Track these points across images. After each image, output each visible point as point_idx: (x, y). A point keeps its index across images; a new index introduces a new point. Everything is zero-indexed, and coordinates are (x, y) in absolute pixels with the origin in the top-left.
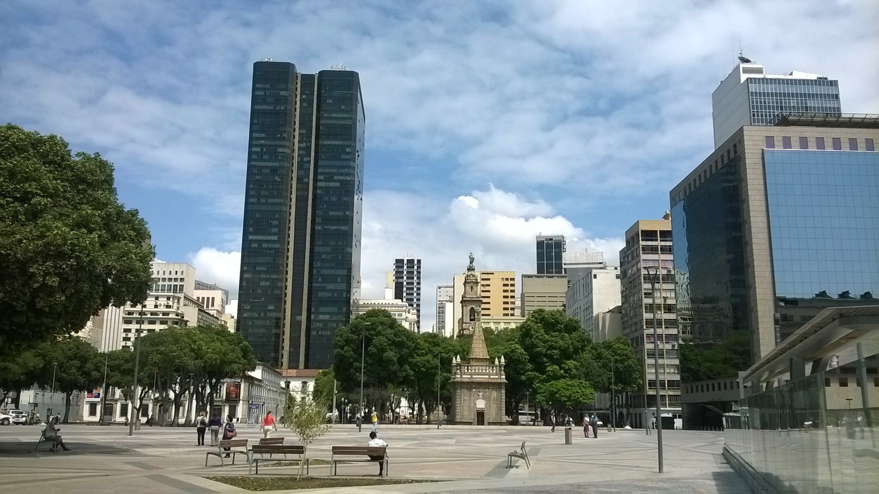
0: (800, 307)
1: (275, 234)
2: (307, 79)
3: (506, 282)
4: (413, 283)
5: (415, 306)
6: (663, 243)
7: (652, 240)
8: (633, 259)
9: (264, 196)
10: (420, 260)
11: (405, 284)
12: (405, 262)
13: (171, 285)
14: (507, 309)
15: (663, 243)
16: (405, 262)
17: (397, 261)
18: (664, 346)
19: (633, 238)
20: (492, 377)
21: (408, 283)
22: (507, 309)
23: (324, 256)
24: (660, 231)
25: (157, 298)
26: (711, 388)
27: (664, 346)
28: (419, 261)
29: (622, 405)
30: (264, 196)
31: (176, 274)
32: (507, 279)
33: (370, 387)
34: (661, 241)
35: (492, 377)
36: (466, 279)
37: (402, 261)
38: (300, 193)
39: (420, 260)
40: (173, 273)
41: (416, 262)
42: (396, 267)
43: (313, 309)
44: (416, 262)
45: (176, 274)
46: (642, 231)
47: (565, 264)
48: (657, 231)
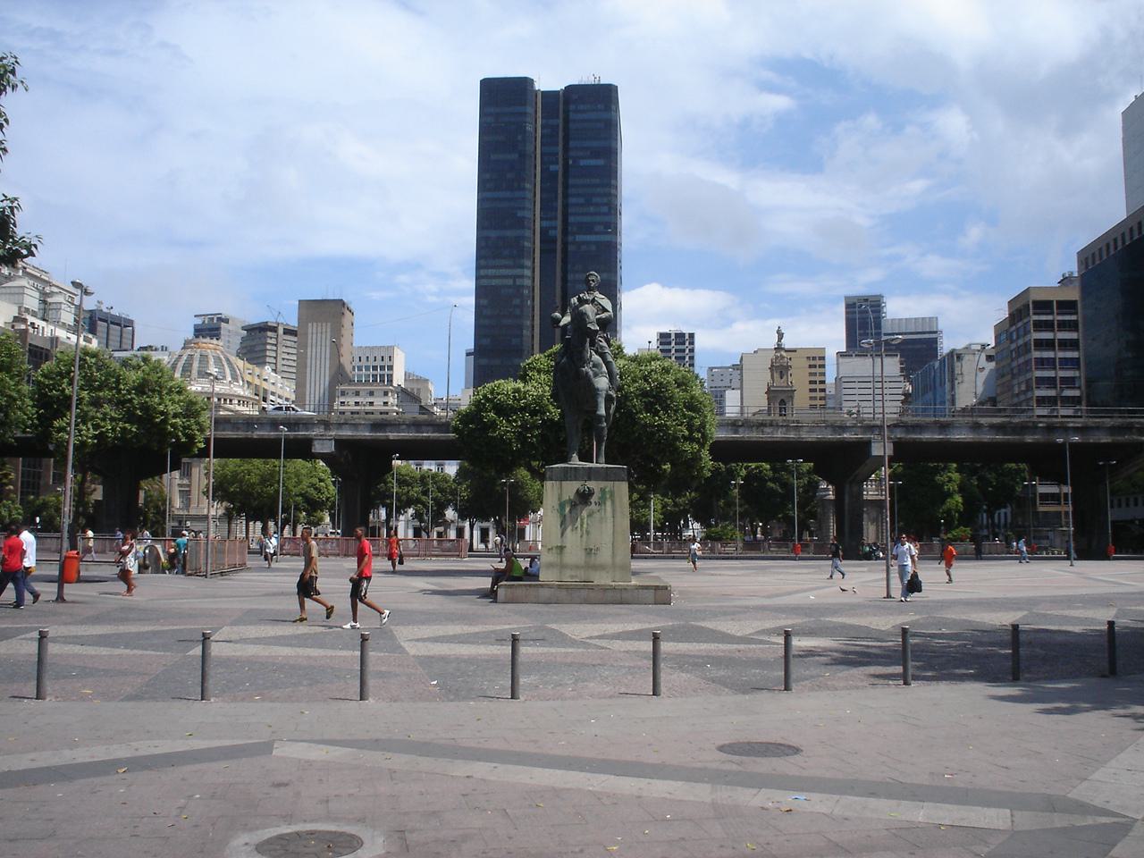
0: (837, 360)
2: (548, 95)
3: (812, 363)
6: (1060, 318)
7: (1071, 314)
8: (1018, 338)
12: (673, 337)
13: (384, 375)
14: (815, 390)
15: (1060, 318)
16: (673, 337)
19: (1019, 311)
20: (870, 493)
22: (815, 390)
24: (1057, 301)
25: (386, 394)
26: (1132, 502)
31: (368, 360)
32: (814, 358)
34: (1058, 314)
35: (870, 493)
36: (772, 363)
37: (669, 335)
38: (544, 121)
40: (379, 358)
41: (687, 337)
44: (687, 337)
45: (368, 360)
46: (1034, 302)
47: (885, 334)
48: (1052, 301)
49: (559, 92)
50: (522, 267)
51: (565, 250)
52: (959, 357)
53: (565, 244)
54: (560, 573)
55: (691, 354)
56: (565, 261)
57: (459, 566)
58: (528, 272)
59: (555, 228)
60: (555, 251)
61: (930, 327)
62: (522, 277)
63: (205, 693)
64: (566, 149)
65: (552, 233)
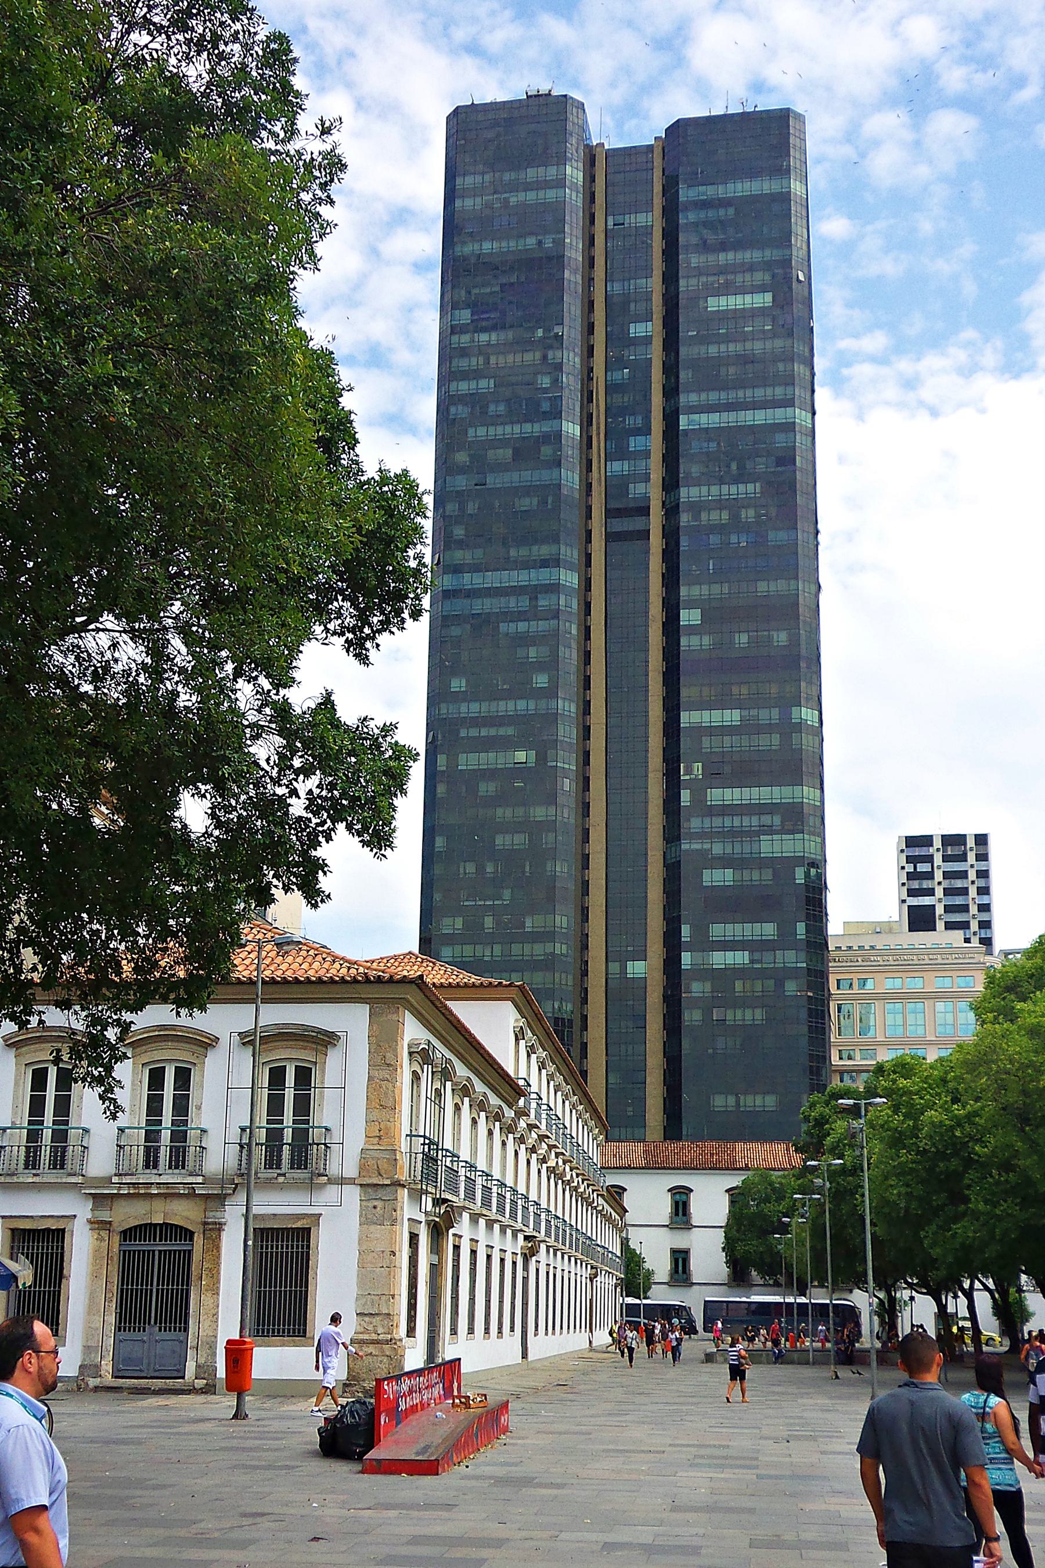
1: (762, 289)
4: (964, 875)
5: (974, 926)
9: (770, 728)
10: (986, 836)
11: (940, 910)
12: (937, 843)
17: (911, 842)
18: (288, 1127)
21: (948, 909)
23: (777, 820)
27: (288, 1127)
28: (982, 840)
29: (767, 266)
30: (770, 728)
33: (319, 844)
37: (926, 841)
39: (986, 836)
41: (971, 843)
42: (909, 859)
43: (685, 930)
44: (971, 843)
49: (650, 148)
50: (554, 562)
51: (671, 534)
52: (504, 1406)
53: (671, 510)
54: (982, 369)
55: (981, 883)
56: (671, 555)
57: (168, 1103)
58: (571, 553)
59: (647, 479)
60: (645, 535)
61: (637, 1358)
62: (554, 588)
63: (111, 1395)
64: (670, 278)
65: (637, 489)
